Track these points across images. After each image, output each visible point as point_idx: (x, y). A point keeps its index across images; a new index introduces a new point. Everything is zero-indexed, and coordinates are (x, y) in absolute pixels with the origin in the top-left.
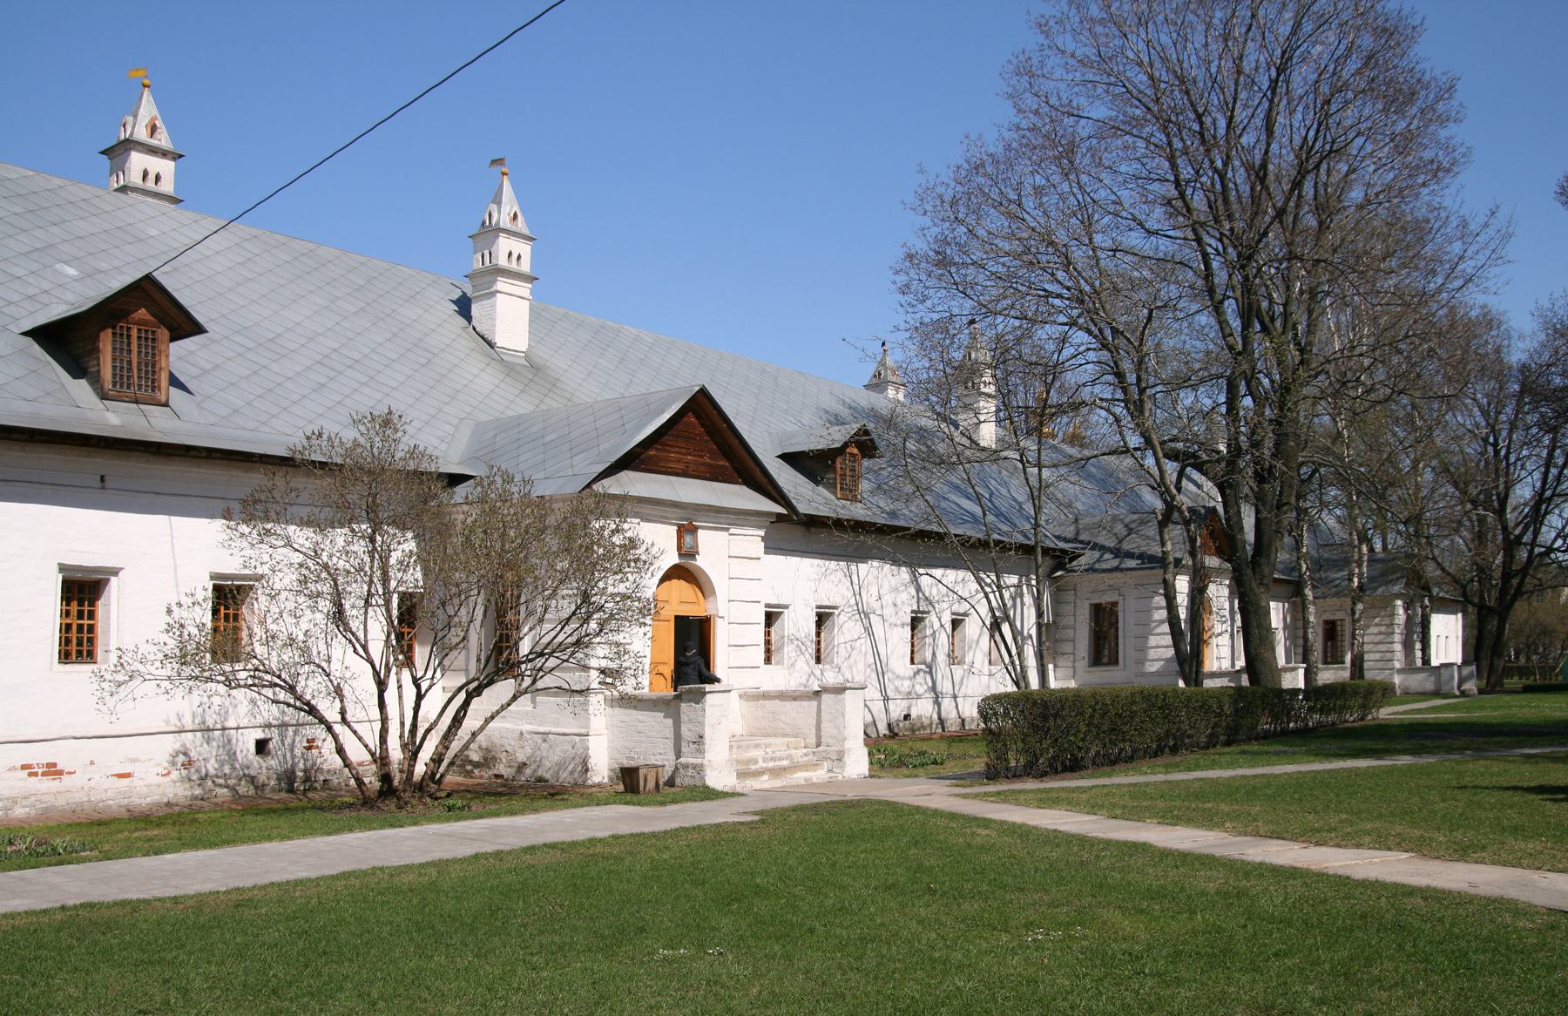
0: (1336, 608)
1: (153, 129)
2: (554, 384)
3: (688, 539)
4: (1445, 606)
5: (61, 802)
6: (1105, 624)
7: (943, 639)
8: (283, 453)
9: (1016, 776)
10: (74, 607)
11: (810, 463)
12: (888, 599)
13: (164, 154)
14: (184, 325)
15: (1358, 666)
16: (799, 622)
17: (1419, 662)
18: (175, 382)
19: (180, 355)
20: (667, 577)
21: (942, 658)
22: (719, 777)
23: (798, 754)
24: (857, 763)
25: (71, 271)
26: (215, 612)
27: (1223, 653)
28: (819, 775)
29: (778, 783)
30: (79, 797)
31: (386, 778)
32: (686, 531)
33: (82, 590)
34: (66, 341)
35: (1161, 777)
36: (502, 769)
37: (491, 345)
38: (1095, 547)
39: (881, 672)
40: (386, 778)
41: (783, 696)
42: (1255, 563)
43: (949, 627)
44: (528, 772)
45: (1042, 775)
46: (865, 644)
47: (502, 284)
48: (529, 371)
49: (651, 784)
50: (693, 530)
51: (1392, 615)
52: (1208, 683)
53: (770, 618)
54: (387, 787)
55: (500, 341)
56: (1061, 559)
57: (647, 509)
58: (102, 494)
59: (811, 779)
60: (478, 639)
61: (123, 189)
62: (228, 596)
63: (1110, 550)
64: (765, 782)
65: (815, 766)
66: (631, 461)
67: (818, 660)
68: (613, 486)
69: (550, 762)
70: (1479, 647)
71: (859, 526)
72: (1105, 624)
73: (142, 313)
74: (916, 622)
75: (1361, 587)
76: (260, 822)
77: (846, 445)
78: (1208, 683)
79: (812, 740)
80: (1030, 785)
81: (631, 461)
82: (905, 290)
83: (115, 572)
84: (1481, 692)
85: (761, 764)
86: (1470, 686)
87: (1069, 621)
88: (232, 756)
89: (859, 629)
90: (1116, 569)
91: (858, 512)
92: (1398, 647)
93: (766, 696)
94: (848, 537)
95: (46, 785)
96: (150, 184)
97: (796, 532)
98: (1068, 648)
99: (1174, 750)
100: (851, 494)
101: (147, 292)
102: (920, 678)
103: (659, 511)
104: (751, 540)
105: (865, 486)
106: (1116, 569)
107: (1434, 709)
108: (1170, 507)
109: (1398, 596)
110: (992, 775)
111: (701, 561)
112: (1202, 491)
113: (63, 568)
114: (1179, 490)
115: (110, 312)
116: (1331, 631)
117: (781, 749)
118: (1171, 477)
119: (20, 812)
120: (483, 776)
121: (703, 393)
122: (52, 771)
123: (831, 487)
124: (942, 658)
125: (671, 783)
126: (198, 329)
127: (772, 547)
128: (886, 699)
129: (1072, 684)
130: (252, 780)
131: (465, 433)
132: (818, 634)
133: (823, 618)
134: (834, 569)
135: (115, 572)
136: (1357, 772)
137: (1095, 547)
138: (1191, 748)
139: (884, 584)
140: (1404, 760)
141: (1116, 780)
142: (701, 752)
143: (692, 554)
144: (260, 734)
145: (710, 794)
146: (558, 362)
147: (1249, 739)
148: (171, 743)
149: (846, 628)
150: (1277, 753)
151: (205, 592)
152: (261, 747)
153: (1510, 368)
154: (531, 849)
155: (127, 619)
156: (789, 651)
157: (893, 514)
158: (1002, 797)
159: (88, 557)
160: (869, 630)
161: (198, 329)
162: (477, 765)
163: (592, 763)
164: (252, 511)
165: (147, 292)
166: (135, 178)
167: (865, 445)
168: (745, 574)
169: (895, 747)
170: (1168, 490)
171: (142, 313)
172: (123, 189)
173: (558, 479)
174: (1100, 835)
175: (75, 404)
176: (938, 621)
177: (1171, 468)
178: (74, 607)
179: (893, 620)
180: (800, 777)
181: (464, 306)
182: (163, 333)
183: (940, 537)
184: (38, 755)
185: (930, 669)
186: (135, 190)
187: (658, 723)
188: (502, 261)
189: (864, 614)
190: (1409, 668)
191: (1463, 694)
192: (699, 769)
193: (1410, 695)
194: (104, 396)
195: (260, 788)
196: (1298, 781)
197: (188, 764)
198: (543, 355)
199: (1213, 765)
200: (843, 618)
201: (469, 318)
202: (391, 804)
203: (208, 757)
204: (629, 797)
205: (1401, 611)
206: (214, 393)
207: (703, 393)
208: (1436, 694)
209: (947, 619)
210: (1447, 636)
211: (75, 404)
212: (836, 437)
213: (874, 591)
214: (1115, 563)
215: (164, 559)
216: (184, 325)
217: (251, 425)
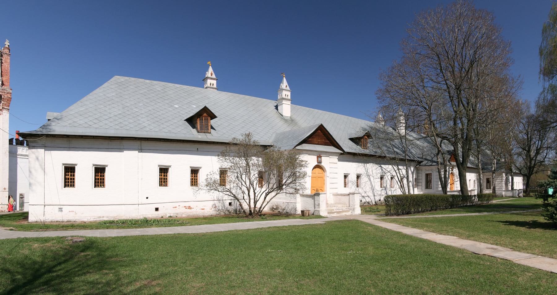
0: (488, 175)
1: (212, 74)
2: (296, 124)
3: (319, 159)
4: (517, 174)
5: (191, 214)
6: (428, 177)
7: (389, 182)
8: (227, 142)
9: (392, 215)
10: (193, 175)
11: (356, 140)
12: (374, 171)
13: (214, 79)
14: (213, 116)
15: (494, 189)
16: (352, 178)
17: (510, 189)
18: (212, 128)
19: (213, 122)
20: (315, 167)
21: (388, 186)
22: (323, 214)
23: (344, 208)
24: (358, 211)
25: (195, 106)
26: (220, 177)
27: (455, 187)
28: (349, 213)
29: (338, 215)
30: (195, 213)
31: (250, 211)
32: (319, 157)
33: (195, 172)
34: (191, 121)
35: (440, 216)
36: (280, 210)
37: (282, 115)
38: (426, 159)
39: (373, 189)
40: (250, 211)
41: (342, 195)
42: (462, 164)
43: (390, 179)
44: (285, 211)
45: (399, 215)
46: (369, 182)
47: (284, 102)
48: (291, 121)
49: (307, 214)
50: (321, 157)
51: (502, 177)
52: (448, 193)
53: (345, 177)
54: (251, 213)
55: (284, 115)
56: (419, 163)
57: (309, 152)
58: (197, 152)
59: (347, 214)
60: (273, 181)
61: (207, 88)
62: (223, 172)
63: (430, 161)
64: (335, 215)
65: (348, 211)
66: (305, 141)
67: (358, 186)
68: (298, 148)
69: (289, 209)
70: (527, 184)
71: (366, 155)
72: (428, 177)
73: (205, 114)
74: (382, 178)
75: (494, 170)
76: (227, 220)
77: (364, 136)
78: (448, 193)
79: (348, 205)
80: (395, 217)
81: (305, 141)
82: (379, 98)
83: (201, 168)
84: (524, 196)
85: (335, 211)
86: (521, 195)
87: (420, 178)
88: (224, 206)
89: (367, 179)
90: (431, 165)
91: (367, 152)
92: (504, 185)
93: (338, 195)
94: (361, 158)
95: (188, 210)
96: (212, 86)
97: (346, 156)
98: (420, 184)
99: (436, 210)
100: (365, 147)
101: (205, 110)
102: (383, 191)
103: (312, 153)
104: (335, 159)
105: (369, 145)
106: (431, 165)
107: (508, 201)
108: (439, 151)
109: (503, 172)
110: (387, 215)
111: (323, 164)
112: (447, 147)
113: (191, 167)
114: (441, 146)
115: (199, 115)
116: (488, 181)
117: (340, 207)
118: (438, 143)
119: (184, 216)
120: (276, 211)
121: (322, 125)
122: (190, 208)
123: (361, 146)
124: (388, 186)
125: (313, 214)
126: (215, 117)
127: (339, 160)
128: (374, 196)
129: (422, 193)
130: (228, 211)
131: (274, 135)
132: (357, 180)
133: (358, 177)
134: (361, 165)
135: (201, 168)
136: (472, 217)
137: (426, 159)
138: (440, 209)
139: (373, 169)
140: (485, 213)
141: (415, 217)
142: (319, 207)
143: (320, 162)
144: (230, 201)
145: (320, 217)
146: (297, 118)
147: (457, 207)
148: (212, 203)
149: (364, 179)
150: (456, 211)
151: (218, 173)
152: (230, 204)
153: (517, 113)
154: (269, 228)
155: (202, 177)
156: (350, 184)
157: (376, 152)
158: (383, 220)
159: (195, 165)
160: (370, 179)
161: (215, 117)
162: (275, 209)
163: (297, 209)
164: (223, 154)
165: (205, 110)
166: (209, 85)
167: (368, 135)
168: (336, 168)
169: (367, 208)
170: (437, 147)
171: (205, 114)
172: (207, 88)
173: (286, 147)
174: (395, 230)
175: (192, 134)
176: (388, 177)
177: (439, 140)
178: (193, 175)
179: (376, 177)
180: (344, 214)
181: (277, 107)
182: (209, 118)
183: (385, 157)
184: (187, 204)
185: (386, 189)
186: (209, 87)
187: (310, 200)
188: (284, 97)
189: (368, 176)
190: (507, 190)
191: (519, 197)
192: (319, 211)
193: (507, 197)
194: (198, 132)
195: (230, 212)
196: (459, 219)
197: (215, 207)
198: (294, 117)
199: (437, 214)
200: (363, 177)
201: (277, 110)
202: (250, 217)
203: (219, 205)
204: (302, 217)
205: (504, 176)
206: (221, 131)
207: (322, 125)
208: (513, 197)
209: (390, 177)
210: (519, 183)
211: (192, 134)
212: (361, 134)
213: (371, 170)
214: (431, 164)
215: (210, 165)
216: (213, 116)
217: (227, 136)
